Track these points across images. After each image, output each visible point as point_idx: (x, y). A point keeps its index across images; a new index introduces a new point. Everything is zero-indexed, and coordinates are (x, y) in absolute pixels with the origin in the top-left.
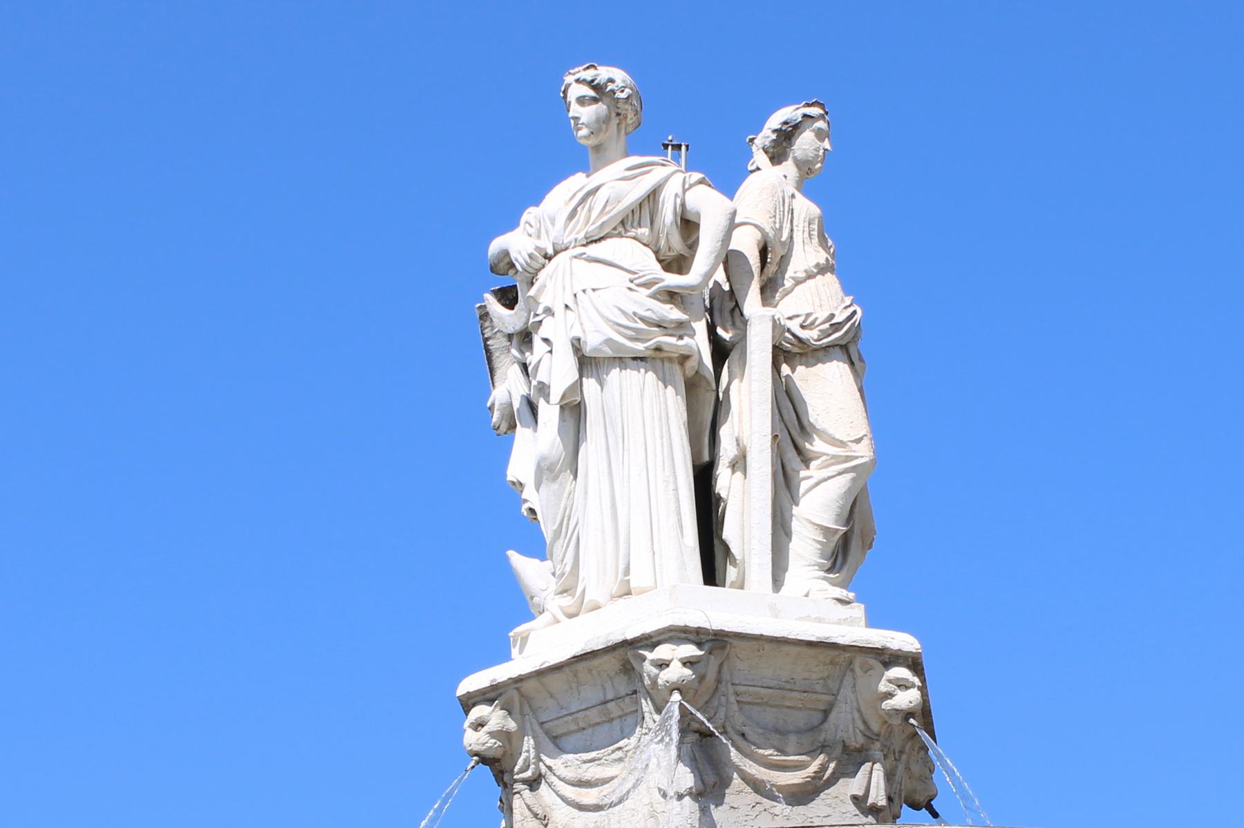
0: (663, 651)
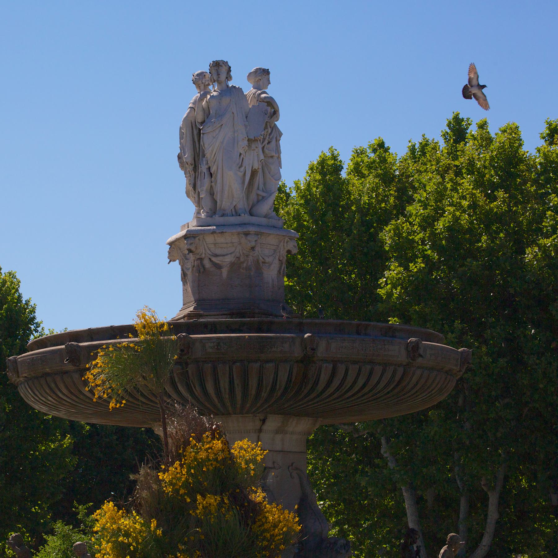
0: (249, 238)
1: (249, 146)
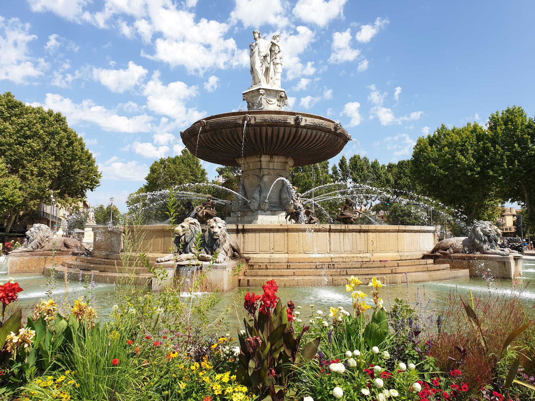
0: (260, 91)
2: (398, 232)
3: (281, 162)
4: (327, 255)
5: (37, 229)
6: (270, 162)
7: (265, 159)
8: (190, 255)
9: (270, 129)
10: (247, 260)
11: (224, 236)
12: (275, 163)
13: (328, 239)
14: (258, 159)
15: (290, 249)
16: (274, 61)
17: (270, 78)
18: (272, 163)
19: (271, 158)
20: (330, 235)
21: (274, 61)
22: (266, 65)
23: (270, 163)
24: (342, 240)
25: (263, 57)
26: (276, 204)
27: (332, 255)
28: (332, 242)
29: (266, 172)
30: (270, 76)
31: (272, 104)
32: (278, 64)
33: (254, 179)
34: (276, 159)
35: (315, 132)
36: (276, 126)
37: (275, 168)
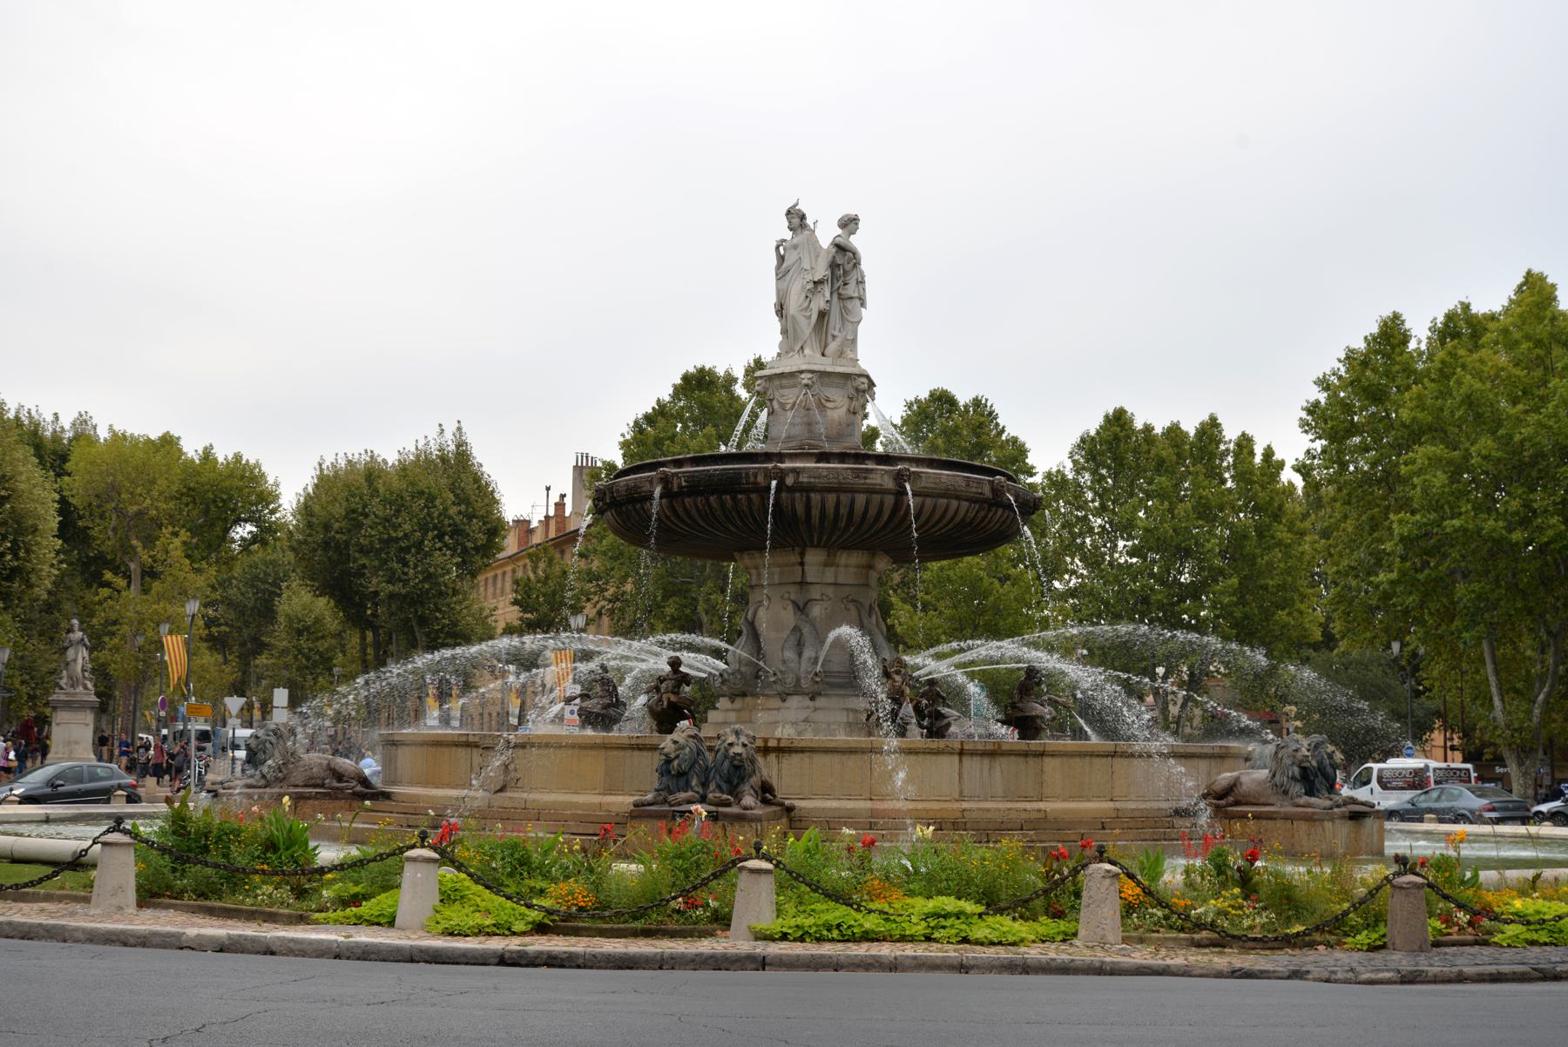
0: (803, 376)
1: (815, 287)
2: (1112, 756)
3: (858, 566)
4: (956, 805)
5: (271, 733)
6: (826, 565)
7: (814, 557)
8: (690, 793)
9: (832, 498)
10: (790, 809)
11: (753, 762)
12: (841, 569)
13: (957, 771)
14: (795, 558)
15: (966, 793)
16: (841, 291)
17: (830, 338)
18: (833, 569)
19: (828, 555)
20: (961, 761)
21: (841, 291)
22: (819, 303)
23: (828, 569)
24: (986, 773)
25: (811, 286)
26: (840, 677)
27: (965, 805)
28: (965, 776)
29: (815, 593)
30: (831, 331)
31: (836, 408)
32: (851, 298)
33: (785, 609)
34: (843, 558)
35: (943, 501)
36: (846, 491)
37: (841, 581)
